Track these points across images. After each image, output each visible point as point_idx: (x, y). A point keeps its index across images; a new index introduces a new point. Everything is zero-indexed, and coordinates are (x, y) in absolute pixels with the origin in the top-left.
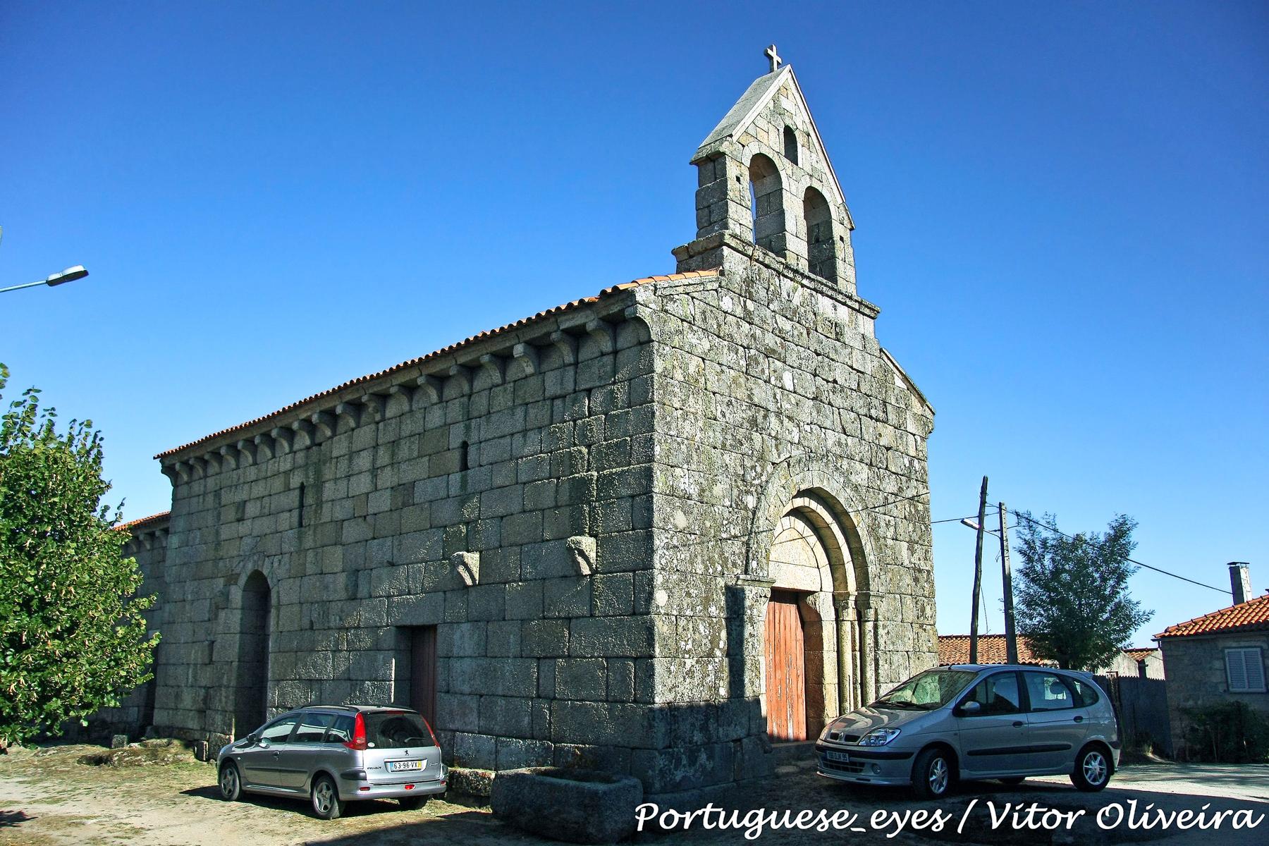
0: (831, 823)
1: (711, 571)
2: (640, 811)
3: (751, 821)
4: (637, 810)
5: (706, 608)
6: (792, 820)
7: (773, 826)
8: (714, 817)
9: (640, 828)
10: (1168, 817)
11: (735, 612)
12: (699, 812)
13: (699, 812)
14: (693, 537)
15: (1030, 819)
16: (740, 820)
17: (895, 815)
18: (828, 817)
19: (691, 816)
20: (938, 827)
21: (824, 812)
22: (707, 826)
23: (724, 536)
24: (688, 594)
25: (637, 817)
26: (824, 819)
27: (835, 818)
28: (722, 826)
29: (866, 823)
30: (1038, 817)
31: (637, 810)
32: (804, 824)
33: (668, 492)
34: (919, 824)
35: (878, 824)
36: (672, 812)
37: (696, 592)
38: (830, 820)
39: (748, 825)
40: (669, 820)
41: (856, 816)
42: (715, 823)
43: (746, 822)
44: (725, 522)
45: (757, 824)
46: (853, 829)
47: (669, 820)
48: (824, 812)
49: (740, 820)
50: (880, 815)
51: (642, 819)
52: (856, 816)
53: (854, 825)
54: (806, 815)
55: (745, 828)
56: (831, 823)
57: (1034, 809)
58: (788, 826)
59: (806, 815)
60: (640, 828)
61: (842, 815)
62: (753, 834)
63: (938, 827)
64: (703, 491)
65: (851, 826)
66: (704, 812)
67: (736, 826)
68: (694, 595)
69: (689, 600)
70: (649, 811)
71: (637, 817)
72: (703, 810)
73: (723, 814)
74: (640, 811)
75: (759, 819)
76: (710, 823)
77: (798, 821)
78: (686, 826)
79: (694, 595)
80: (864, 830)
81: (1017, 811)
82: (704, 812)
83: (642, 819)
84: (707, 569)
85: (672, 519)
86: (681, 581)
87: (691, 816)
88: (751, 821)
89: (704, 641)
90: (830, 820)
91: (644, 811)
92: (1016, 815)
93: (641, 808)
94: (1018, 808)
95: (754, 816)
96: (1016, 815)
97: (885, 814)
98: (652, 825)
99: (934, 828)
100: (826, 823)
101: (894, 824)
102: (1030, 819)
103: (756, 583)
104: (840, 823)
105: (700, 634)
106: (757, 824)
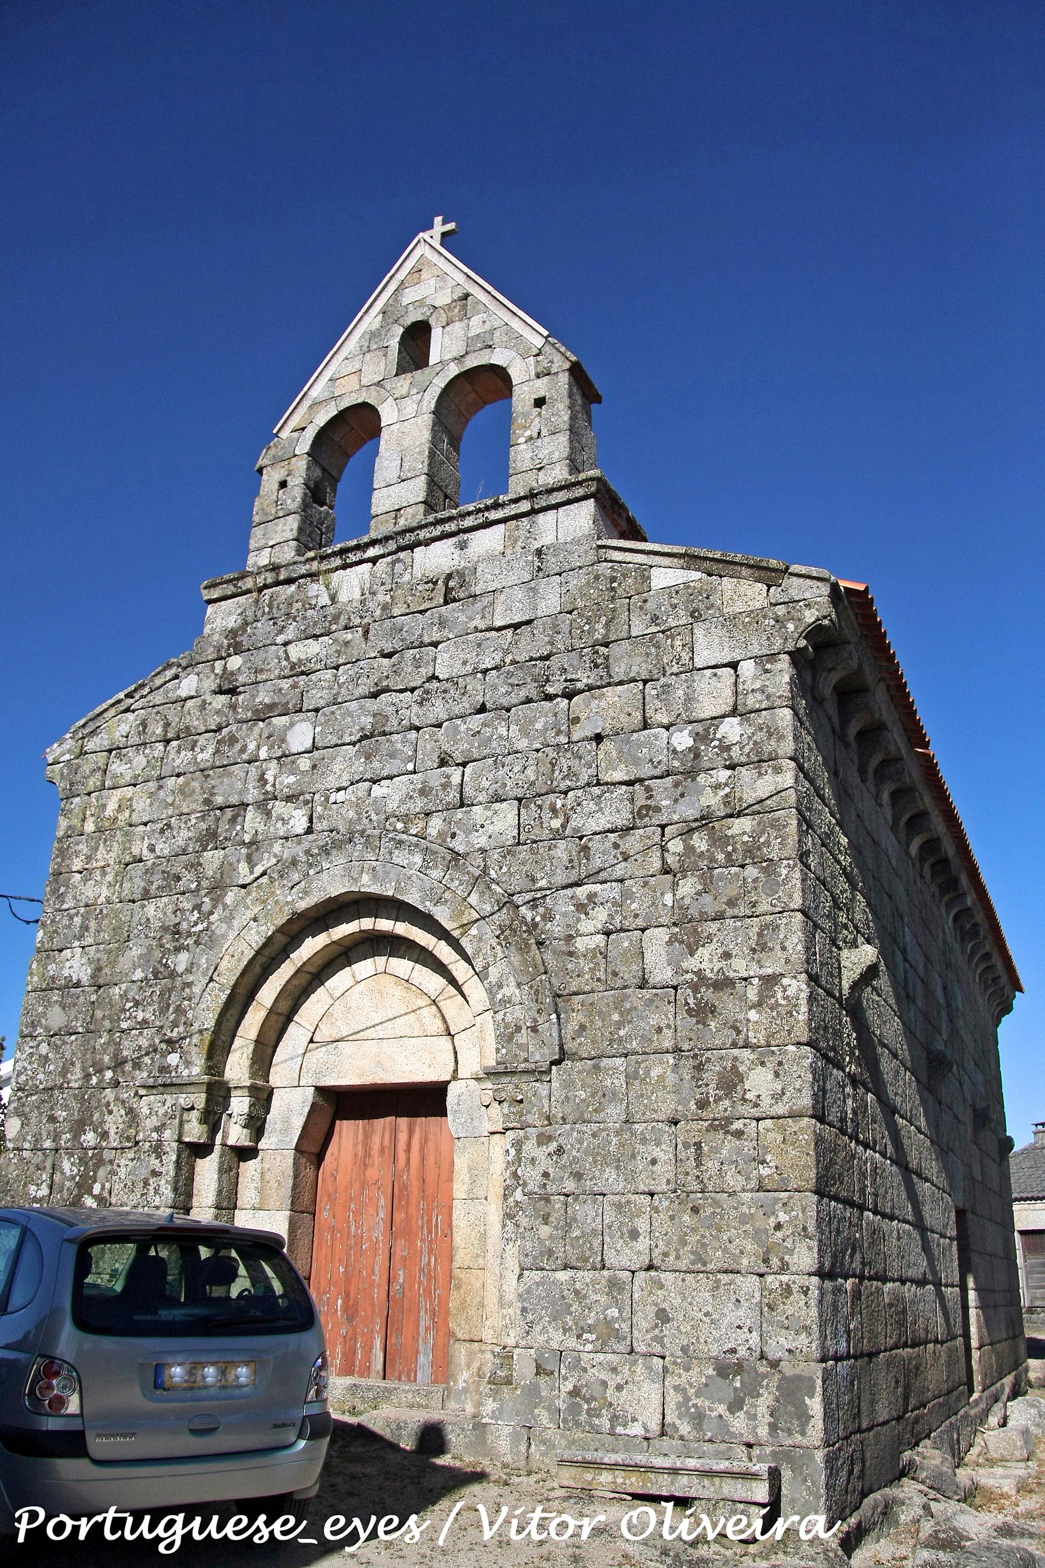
0: (272, 1533)
1: (94, 1080)
2: (21, 1516)
3: (166, 1530)
4: (17, 1515)
5: (76, 1137)
6: (220, 1529)
7: (197, 1536)
8: (118, 1524)
9: (21, 1539)
10: (714, 1525)
11: (128, 1139)
12: (99, 1518)
13: (99, 1518)
14: (73, 1037)
15: (533, 1527)
16: (152, 1528)
17: (357, 1522)
18: (268, 1524)
19: (88, 1522)
20: (261, 1538)
21: (263, 1518)
22: (109, 1536)
23: (124, 1025)
24: (52, 1119)
25: (17, 1524)
26: (263, 1527)
27: (277, 1526)
28: (128, 1537)
29: (319, 1534)
30: (542, 1527)
31: (17, 1515)
32: (236, 1533)
33: (44, 986)
34: (334, 1533)
35: (334, 1533)
36: (63, 1517)
37: (64, 1114)
38: (270, 1529)
39: (163, 1535)
40: (59, 1528)
41: (305, 1523)
42: (120, 1533)
43: (160, 1531)
44: (129, 1005)
45: (174, 1533)
46: (301, 1541)
47: (59, 1528)
48: (263, 1518)
49: (152, 1528)
50: (336, 1522)
51: (23, 1527)
52: (305, 1523)
53: (301, 1535)
54: (239, 1522)
55: (158, 1539)
56: (272, 1533)
57: (538, 1514)
58: (216, 1536)
59: (239, 1522)
60: (21, 1539)
61: (286, 1522)
62: (169, 1547)
63: (261, 1538)
64: (99, 969)
65: (298, 1536)
66: (105, 1518)
67: (148, 1536)
68: (61, 1119)
69: (51, 1127)
70: (33, 1516)
71: (17, 1524)
72: (104, 1515)
73: (130, 1520)
74: (21, 1516)
75: (178, 1527)
76: (113, 1532)
77: (229, 1530)
78: (82, 1536)
79: (61, 1119)
80: (315, 1542)
81: (515, 1517)
82: (105, 1518)
83: (23, 1527)
84: (87, 1076)
85: (43, 1021)
86: (44, 1101)
87: (88, 1522)
88: (166, 1530)
89: (67, 1184)
90: (270, 1529)
91: (26, 1517)
92: (515, 1522)
93: (23, 1513)
94: (517, 1512)
95: (171, 1524)
96: (515, 1522)
97: (342, 1520)
98: (37, 1534)
99: (256, 1539)
100: (265, 1532)
101: (355, 1532)
102: (533, 1527)
103: (173, 1089)
104: (284, 1533)
105: (62, 1173)
106: (174, 1533)
